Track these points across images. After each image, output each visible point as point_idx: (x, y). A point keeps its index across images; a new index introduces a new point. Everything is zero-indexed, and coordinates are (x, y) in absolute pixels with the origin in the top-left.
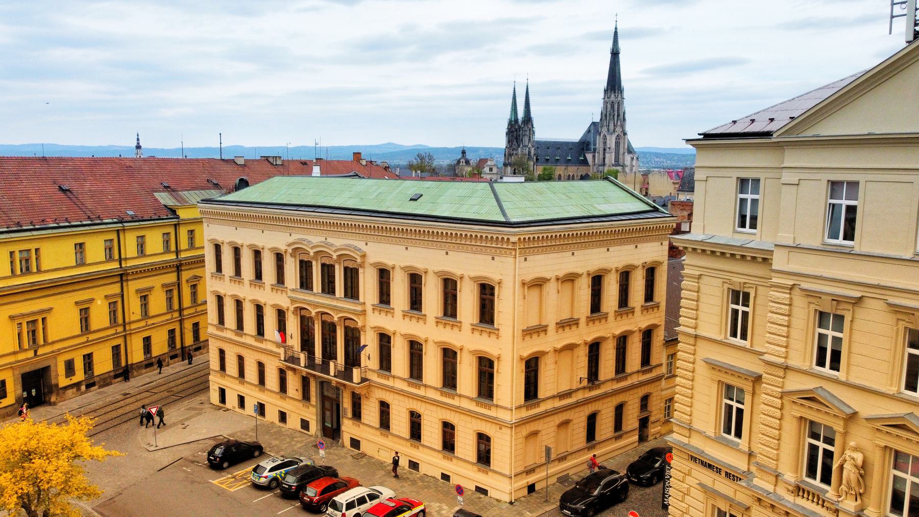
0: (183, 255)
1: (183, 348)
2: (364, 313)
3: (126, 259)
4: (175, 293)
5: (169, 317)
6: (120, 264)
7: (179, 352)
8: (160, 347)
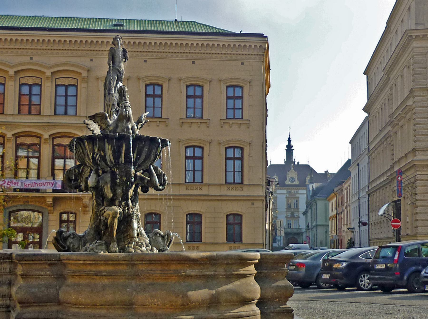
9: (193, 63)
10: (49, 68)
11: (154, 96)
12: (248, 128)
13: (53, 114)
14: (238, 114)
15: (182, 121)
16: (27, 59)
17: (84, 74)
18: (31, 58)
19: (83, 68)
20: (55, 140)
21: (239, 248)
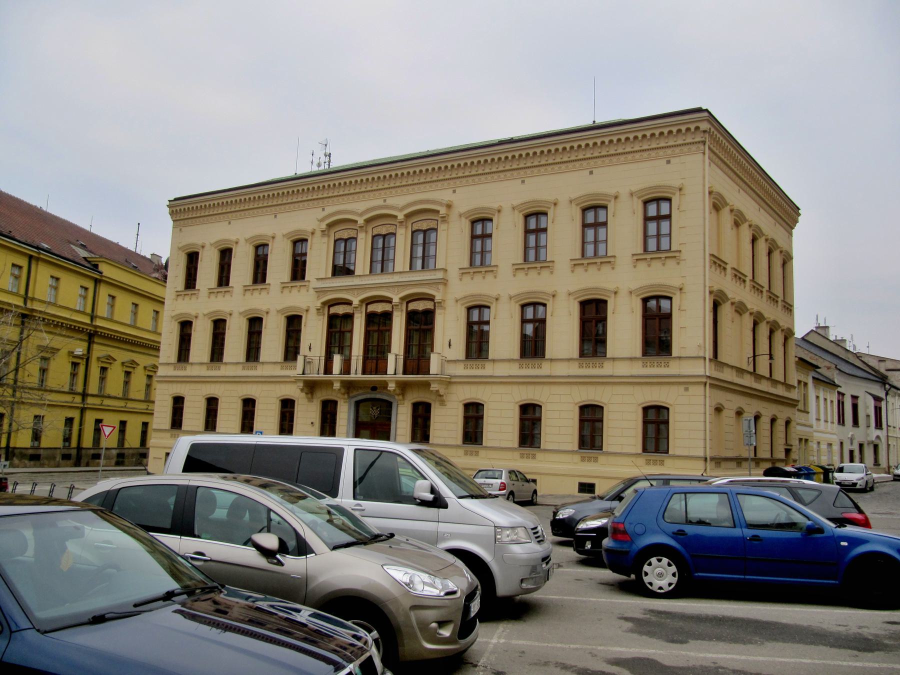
0: (98, 323)
1: (79, 448)
2: (444, 282)
3: (33, 299)
4: (82, 369)
5: (69, 398)
6: (25, 303)
7: (74, 452)
8: (52, 438)
9: (591, 173)
10: (401, 210)
11: (659, 218)
12: (678, 263)
13: (368, 272)
14: (664, 245)
15: (636, 257)
16: (380, 202)
17: (443, 211)
18: (385, 201)
19: (441, 204)
20: (410, 305)
21: (662, 463)
